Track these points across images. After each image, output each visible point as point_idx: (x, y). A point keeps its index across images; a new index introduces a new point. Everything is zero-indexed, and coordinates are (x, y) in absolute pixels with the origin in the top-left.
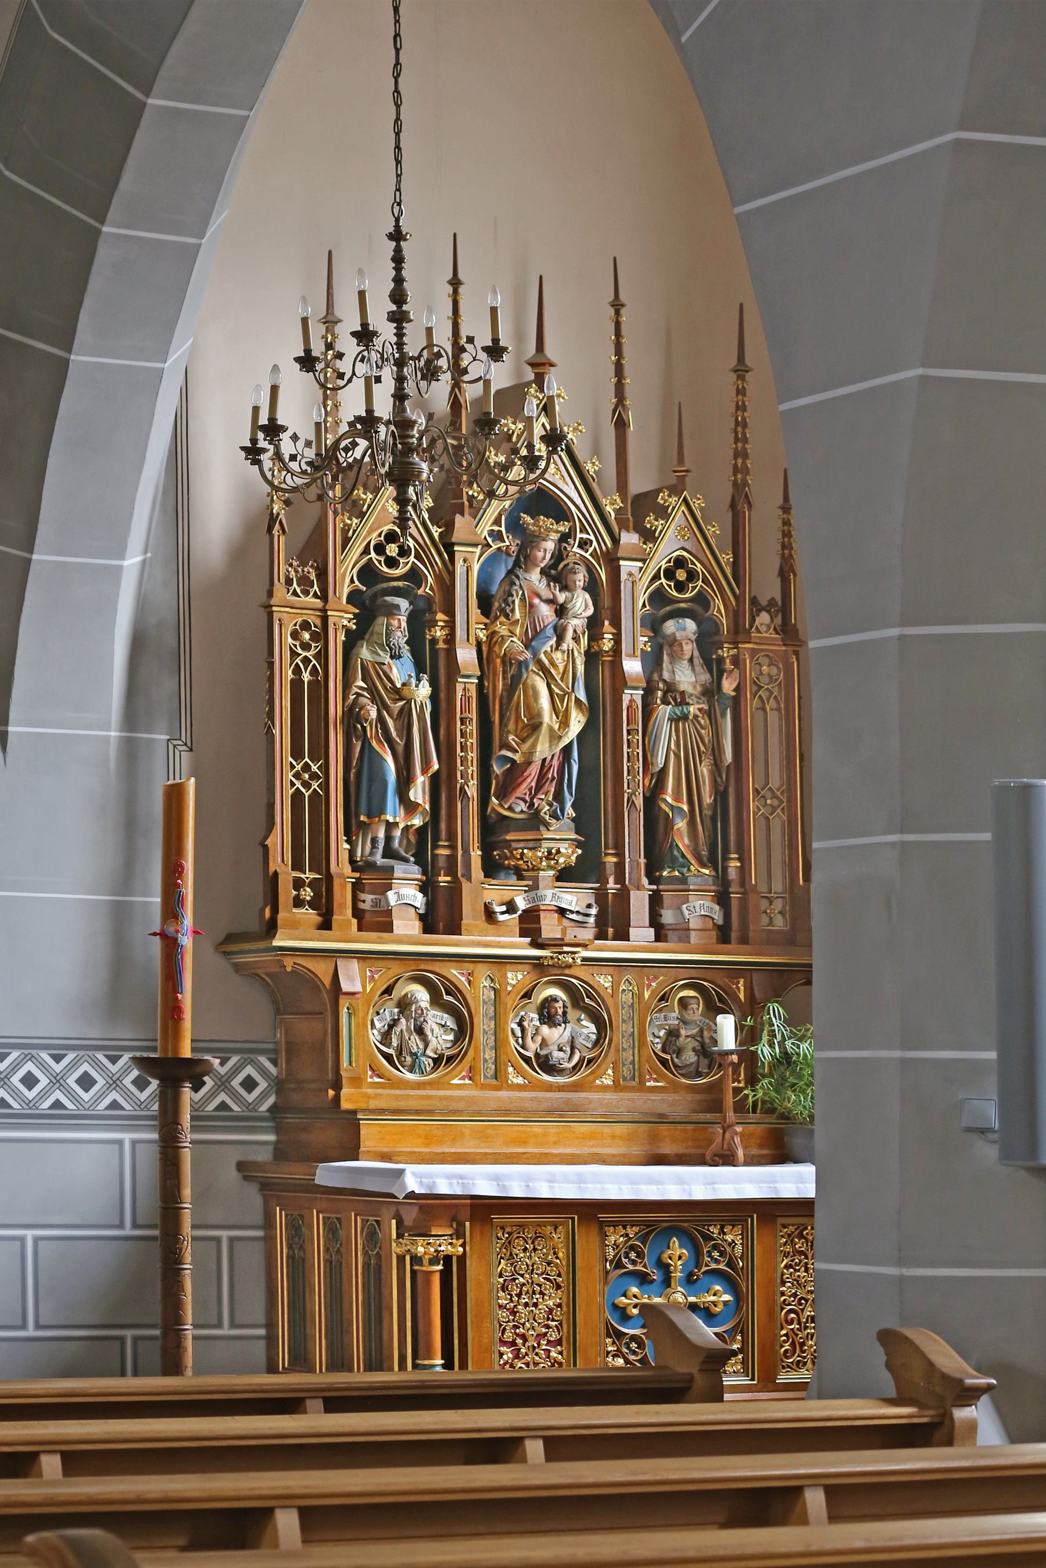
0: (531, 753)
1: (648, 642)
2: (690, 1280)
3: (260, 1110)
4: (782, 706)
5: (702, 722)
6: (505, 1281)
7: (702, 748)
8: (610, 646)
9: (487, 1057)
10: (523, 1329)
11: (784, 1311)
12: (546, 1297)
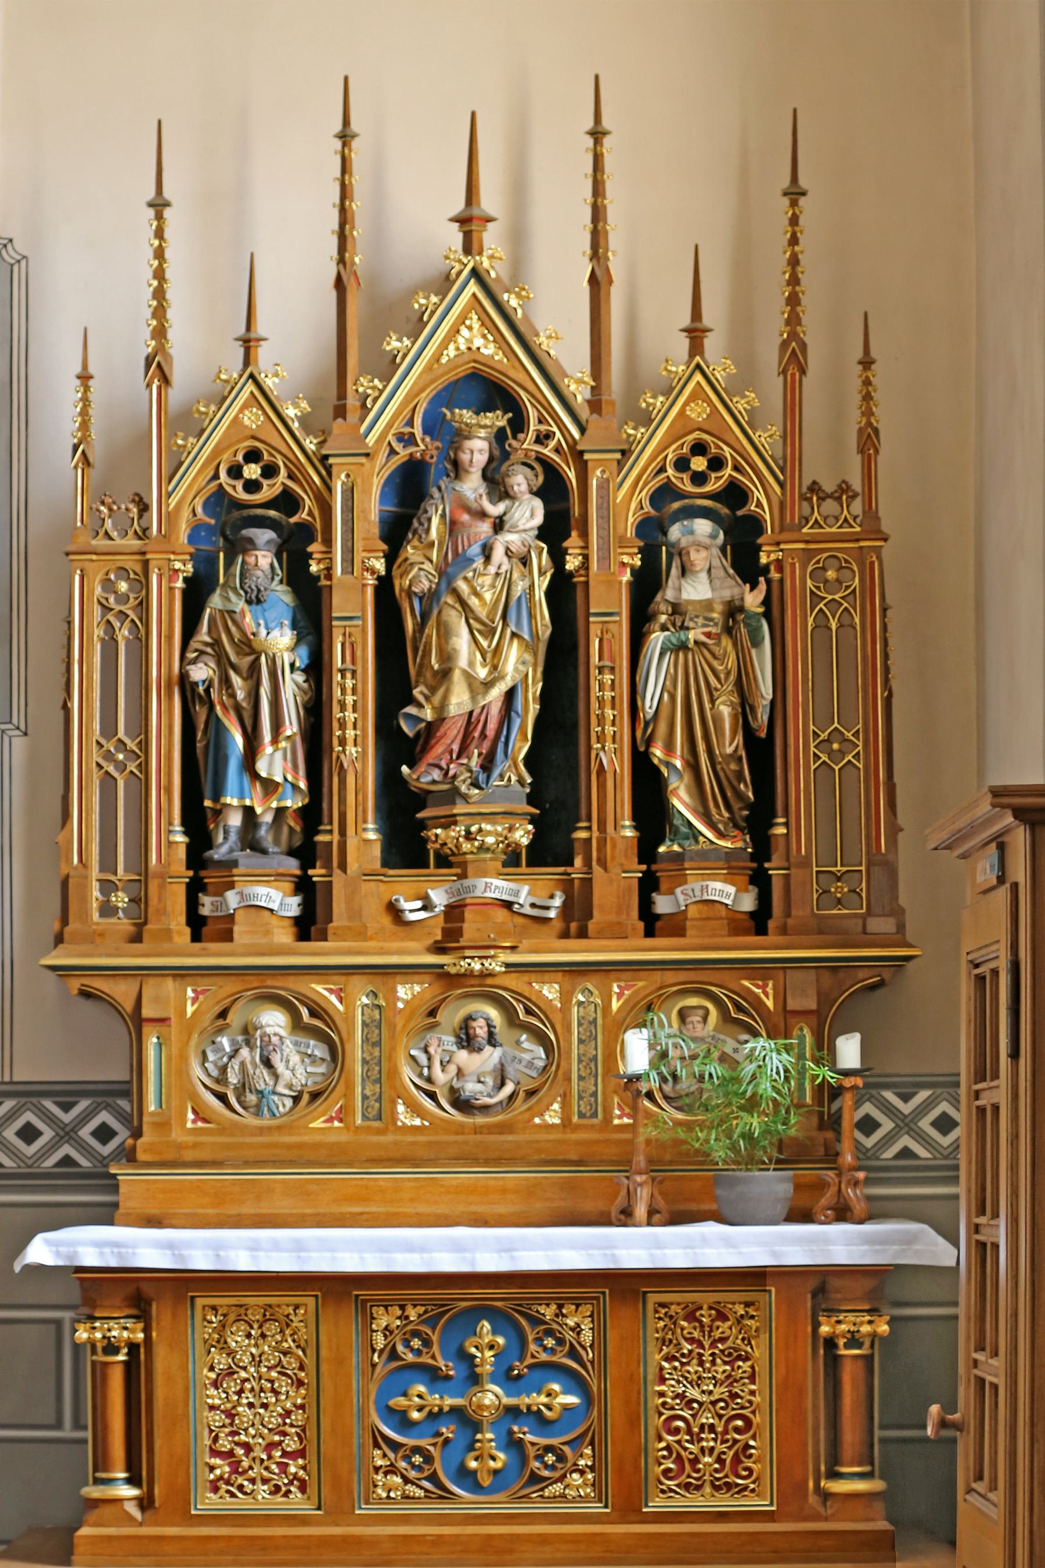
0: (441, 710)
2: (509, 1378)
4: (857, 620)
6: (218, 1375)
8: (577, 563)
9: (368, 1092)
10: (246, 1435)
11: (663, 1418)
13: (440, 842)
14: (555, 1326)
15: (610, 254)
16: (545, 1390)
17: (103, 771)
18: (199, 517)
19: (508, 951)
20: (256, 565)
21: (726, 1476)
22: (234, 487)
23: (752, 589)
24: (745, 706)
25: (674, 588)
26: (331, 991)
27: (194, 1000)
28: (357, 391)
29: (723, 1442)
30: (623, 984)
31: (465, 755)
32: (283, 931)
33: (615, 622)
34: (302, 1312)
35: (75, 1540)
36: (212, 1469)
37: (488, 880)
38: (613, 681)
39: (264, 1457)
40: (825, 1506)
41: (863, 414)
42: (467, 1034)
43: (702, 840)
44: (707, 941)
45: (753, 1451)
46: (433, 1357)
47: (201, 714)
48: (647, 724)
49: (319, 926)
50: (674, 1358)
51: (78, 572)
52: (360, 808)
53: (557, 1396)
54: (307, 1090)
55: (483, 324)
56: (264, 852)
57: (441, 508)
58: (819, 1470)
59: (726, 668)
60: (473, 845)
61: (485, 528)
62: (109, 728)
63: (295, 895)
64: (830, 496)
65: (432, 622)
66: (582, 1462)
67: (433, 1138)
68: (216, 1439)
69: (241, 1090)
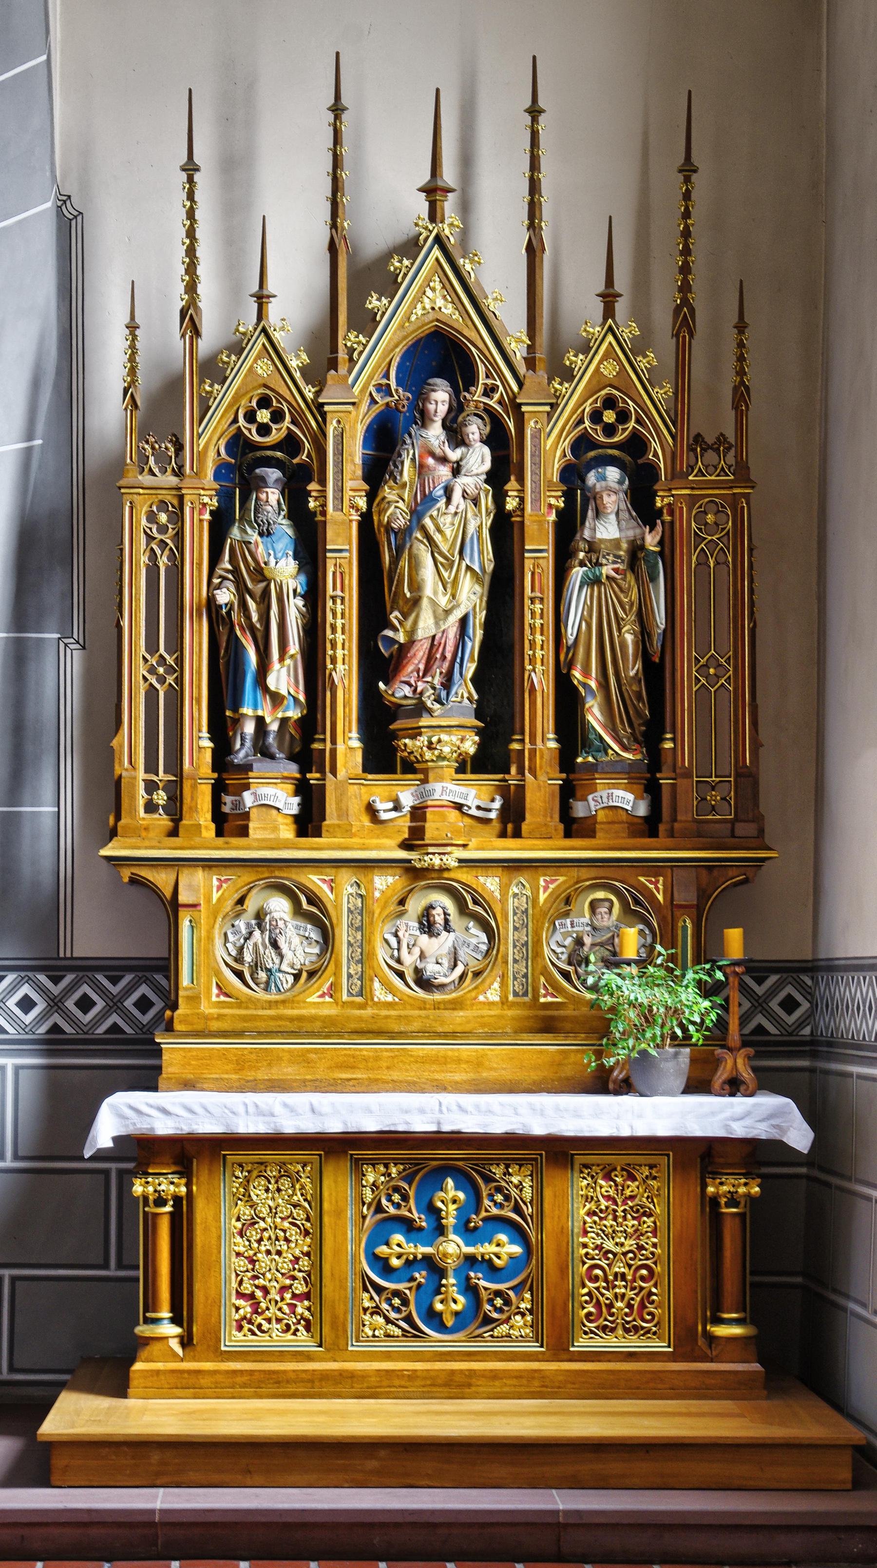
0: (411, 633)
1: (561, 497)
2: (467, 1230)
3: (96, 1032)
4: (730, 559)
6: (244, 1225)
9: (352, 972)
10: (264, 1280)
11: (586, 1266)
12: (293, 1245)
14: (503, 1184)
15: (543, 224)
16: (495, 1240)
17: (148, 683)
19: (461, 848)
20: (267, 501)
21: (634, 1320)
22: (250, 430)
23: (650, 531)
26: (324, 881)
27: (219, 888)
28: (346, 345)
29: (633, 1289)
30: (548, 878)
31: (429, 674)
32: (287, 828)
33: (543, 558)
34: (309, 1168)
35: (131, 1375)
36: (238, 1309)
37: (444, 784)
38: (542, 610)
39: (278, 1298)
40: (710, 1347)
41: (737, 373)
42: (428, 921)
43: (610, 752)
44: (611, 843)
45: (654, 1297)
46: (410, 1211)
47: (223, 630)
48: (568, 648)
49: (314, 824)
50: (595, 1213)
51: (128, 504)
53: (504, 1246)
54: (305, 968)
55: (444, 287)
56: (272, 757)
57: (411, 452)
58: (706, 1315)
59: (630, 600)
60: (433, 754)
61: (444, 472)
62: (151, 646)
63: (296, 795)
64: (710, 447)
65: (406, 555)
66: (523, 1305)
67: (402, 1013)
68: (241, 1283)
69: (255, 967)
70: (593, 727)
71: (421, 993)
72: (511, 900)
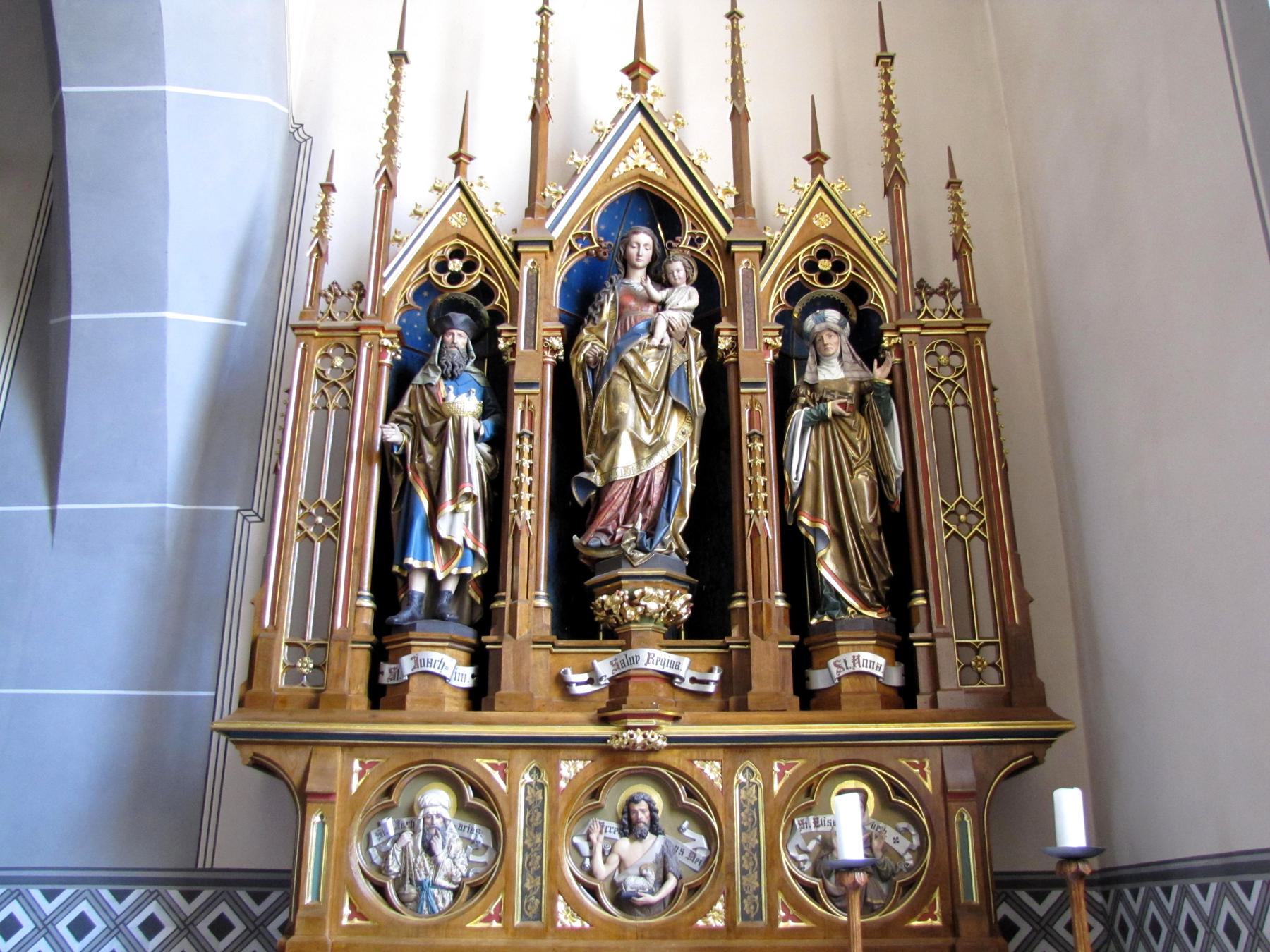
4: (970, 399)
5: (852, 422)
7: (852, 453)
8: (727, 344)
13: (606, 609)
18: (409, 303)
24: (881, 478)
25: (811, 373)
26: (494, 766)
27: (361, 774)
30: (783, 763)
31: (630, 521)
32: (457, 702)
42: (630, 820)
43: (850, 609)
47: (397, 481)
52: (533, 571)
55: (647, 148)
64: (935, 292)
70: (828, 583)
71: (620, 918)
72: (736, 791)
